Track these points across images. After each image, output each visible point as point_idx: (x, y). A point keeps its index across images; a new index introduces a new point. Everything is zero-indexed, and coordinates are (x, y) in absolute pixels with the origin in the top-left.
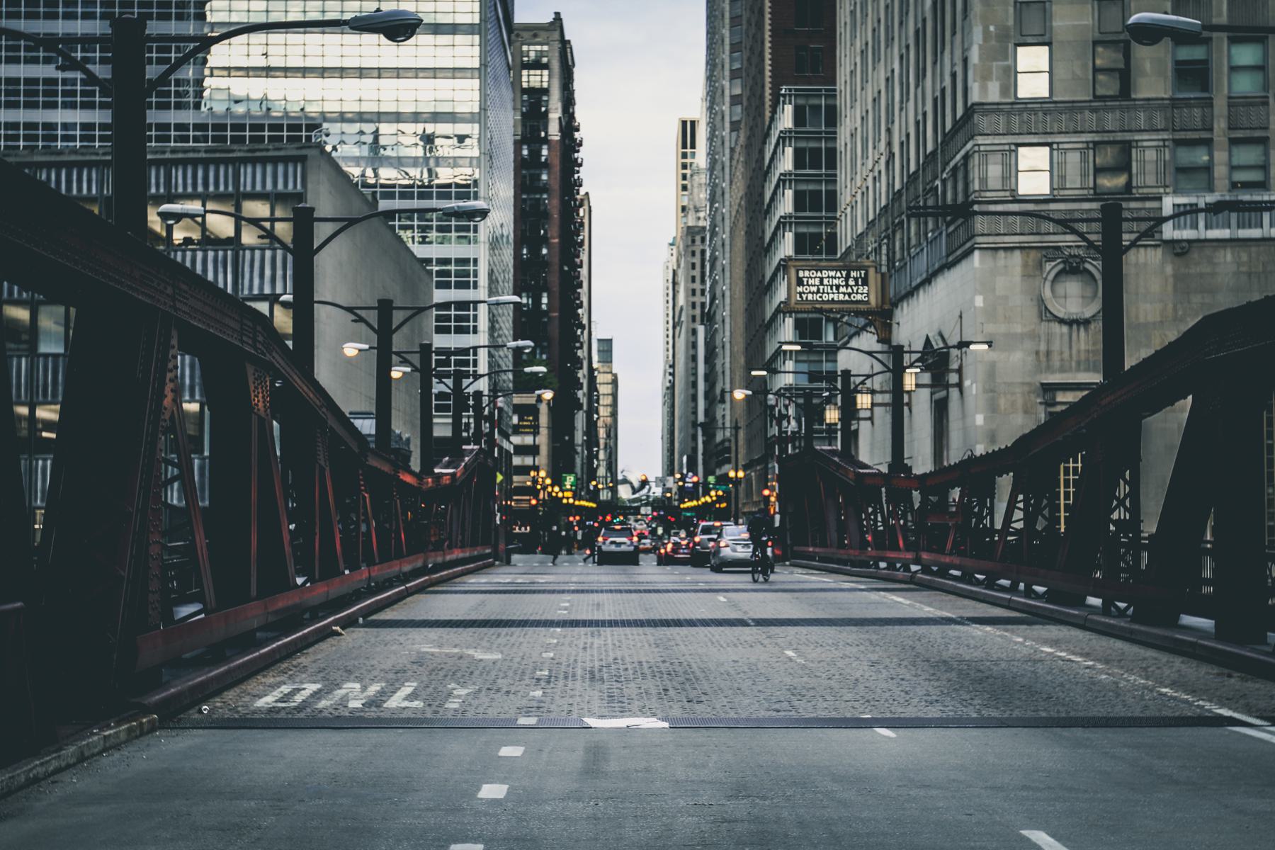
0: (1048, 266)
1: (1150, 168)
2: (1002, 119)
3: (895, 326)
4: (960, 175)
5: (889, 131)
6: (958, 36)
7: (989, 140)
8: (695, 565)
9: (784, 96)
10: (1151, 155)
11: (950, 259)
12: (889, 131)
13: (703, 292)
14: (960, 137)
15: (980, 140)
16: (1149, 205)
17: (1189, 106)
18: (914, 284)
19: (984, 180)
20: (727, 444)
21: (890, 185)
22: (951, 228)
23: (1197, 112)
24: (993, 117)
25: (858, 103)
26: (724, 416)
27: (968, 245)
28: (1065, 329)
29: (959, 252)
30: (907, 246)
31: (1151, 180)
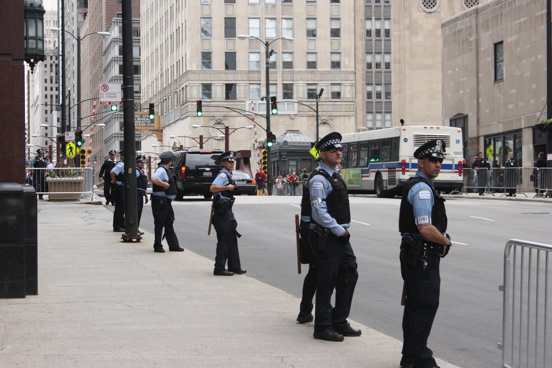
0: (211, 122)
1: (242, 92)
2: (197, 76)
3: (164, 136)
4: (184, 90)
5: (161, 65)
6: (184, 45)
7: (193, 82)
8: (405, 247)
9: (114, 22)
10: (242, 88)
11: (182, 117)
12: (161, 65)
13: (57, 89)
14: (184, 79)
15: (190, 82)
16: (242, 103)
17: (254, 73)
18: (170, 122)
19: (191, 95)
20: (81, 165)
21: (162, 84)
22: (182, 107)
23: (256, 75)
24: (194, 75)
25: (150, 47)
26: (74, 122)
27: (187, 114)
28: (216, 141)
29: (184, 116)
30: (167, 108)
31: (242, 96)
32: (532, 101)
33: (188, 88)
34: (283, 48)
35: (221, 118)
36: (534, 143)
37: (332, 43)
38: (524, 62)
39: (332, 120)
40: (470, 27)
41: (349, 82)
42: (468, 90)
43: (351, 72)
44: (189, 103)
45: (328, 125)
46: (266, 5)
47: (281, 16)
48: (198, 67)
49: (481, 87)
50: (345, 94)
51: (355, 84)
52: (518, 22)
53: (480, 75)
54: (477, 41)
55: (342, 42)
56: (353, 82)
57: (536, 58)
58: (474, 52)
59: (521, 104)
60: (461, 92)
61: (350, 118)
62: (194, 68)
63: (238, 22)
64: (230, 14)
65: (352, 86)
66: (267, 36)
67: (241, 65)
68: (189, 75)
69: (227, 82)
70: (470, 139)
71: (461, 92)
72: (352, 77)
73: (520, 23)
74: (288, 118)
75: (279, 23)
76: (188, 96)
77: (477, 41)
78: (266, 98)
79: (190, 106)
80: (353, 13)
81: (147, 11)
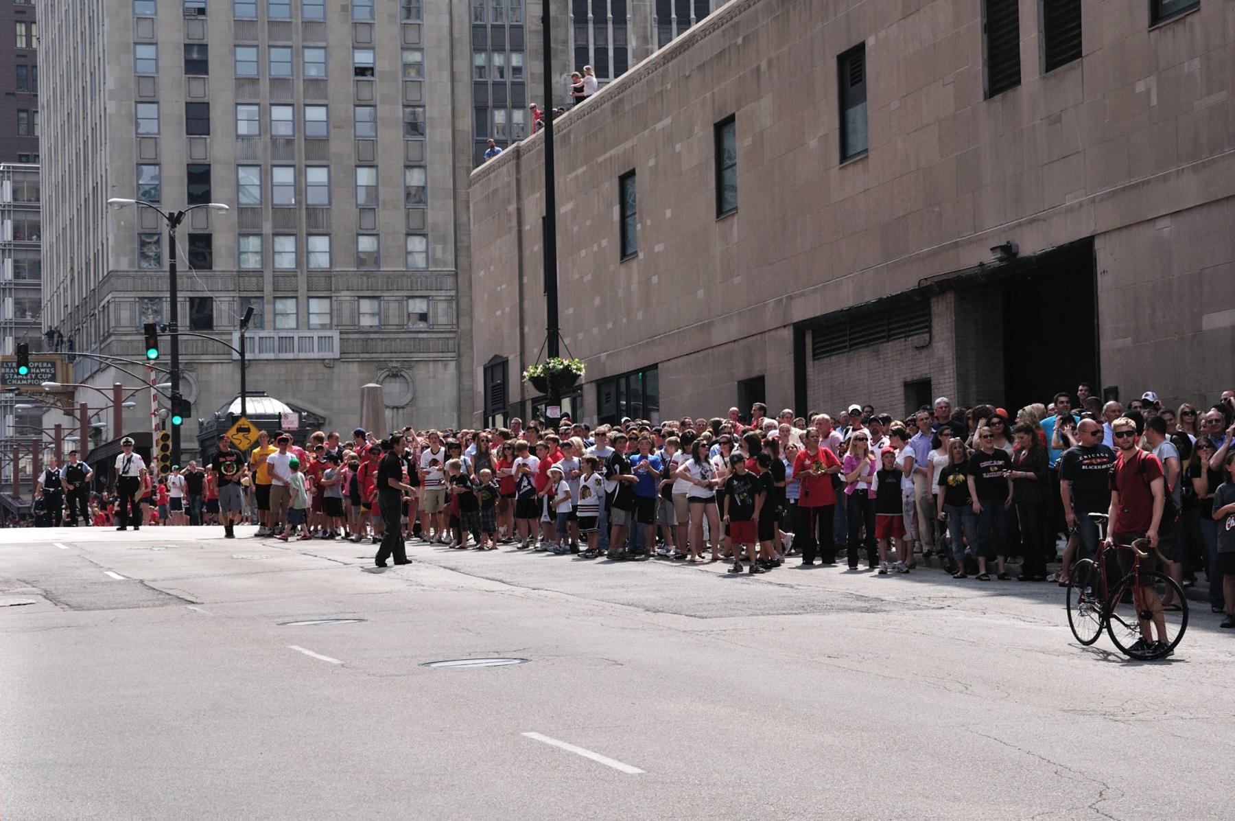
1: (225, 315)
2: (130, 282)
7: (121, 295)
15: (116, 294)
19: (118, 320)
23: (254, 280)
31: (225, 321)
32: (595, 331)
33: (112, 307)
34: (309, 226)
35: (398, 365)
36: (599, 414)
37: (408, 216)
38: (583, 253)
39: (410, 368)
40: (509, 184)
41: (443, 293)
42: (507, 310)
43: (448, 274)
44: (113, 338)
45: (402, 380)
46: (274, 140)
47: (304, 162)
48: (131, 264)
49: (526, 304)
50: (436, 316)
51: (457, 296)
52: (574, 174)
53: (525, 280)
54: (519, 211)
55: (430, 213)
56: (453, 293)
57: (599, 245)
58: (514, 232)
59: (580, 336)
60: (499, 313)
61: (446, 366)
62: (124, 265)
63: (216, 174)
64: (199, 155)
65: (449, 300)
66: (275, 202)
67: (222, 261)
68: (112, 280)
69: (191, 294)
70: (512, 405)
71: (499, 313)
72: (450, 282)
73: (577, 177)
74: (320, 367)
75: (266, 173)
76: (112, 324)
77: (519, 211)
78: (170, 326)
79: (114, 344)
80: (450, 156)
81: (50, 149)
